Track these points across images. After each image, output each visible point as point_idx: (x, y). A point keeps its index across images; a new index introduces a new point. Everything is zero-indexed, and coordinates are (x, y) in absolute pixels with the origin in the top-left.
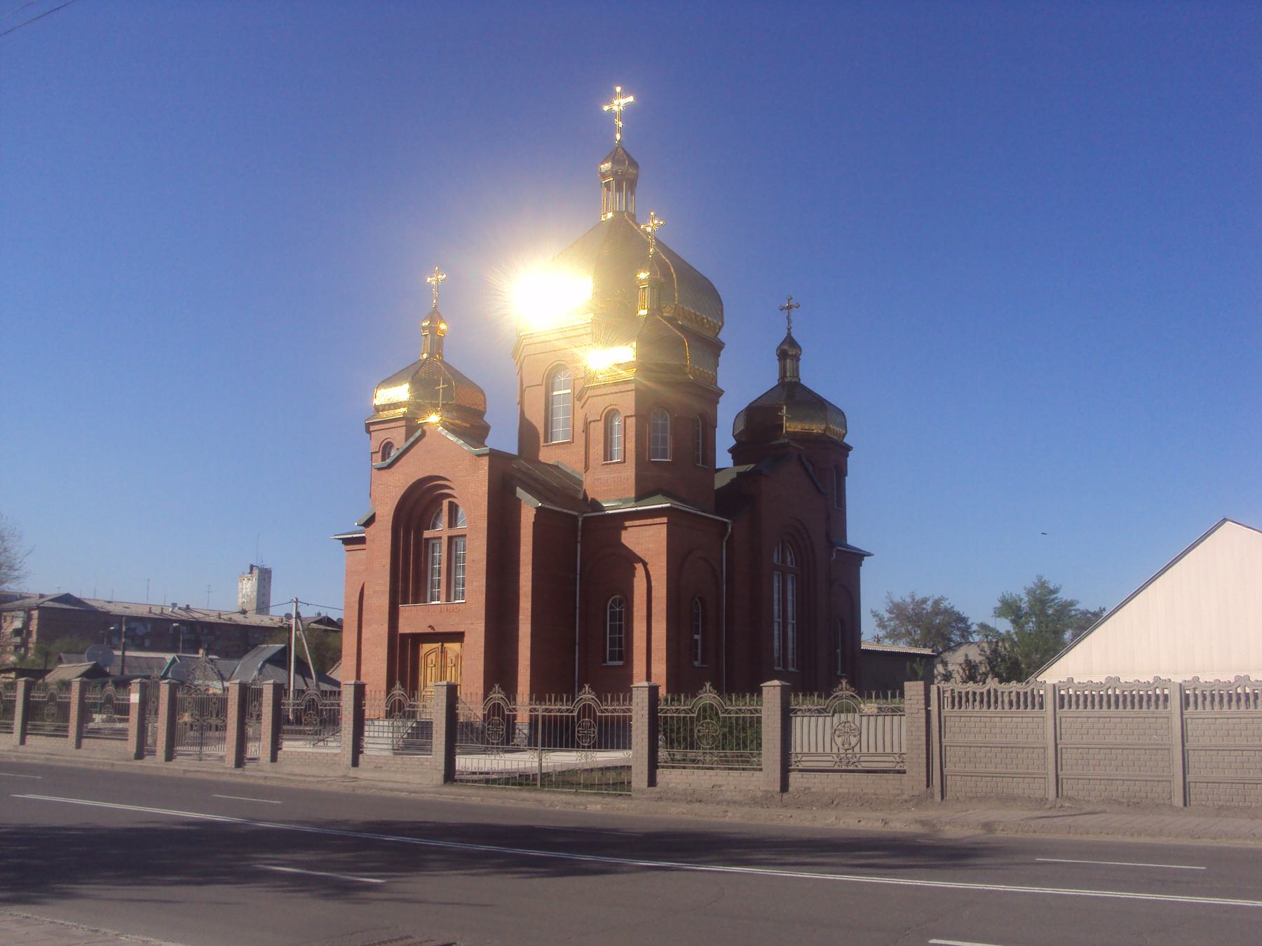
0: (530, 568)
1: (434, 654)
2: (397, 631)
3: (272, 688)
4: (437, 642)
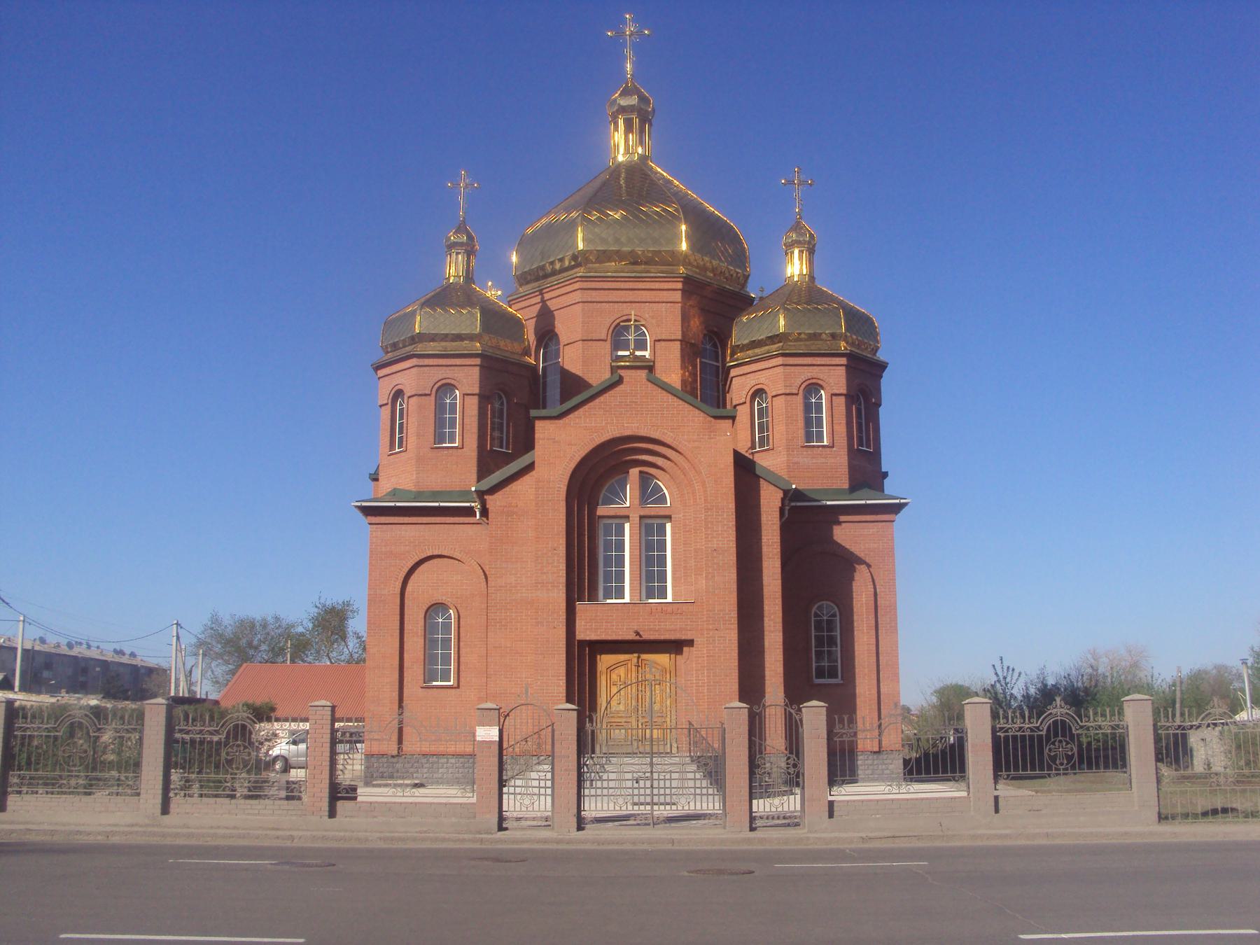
0: (777, 564)
1: (623, 668)
2: (575, 638)
3: (165, 711)
4: (632, 653)
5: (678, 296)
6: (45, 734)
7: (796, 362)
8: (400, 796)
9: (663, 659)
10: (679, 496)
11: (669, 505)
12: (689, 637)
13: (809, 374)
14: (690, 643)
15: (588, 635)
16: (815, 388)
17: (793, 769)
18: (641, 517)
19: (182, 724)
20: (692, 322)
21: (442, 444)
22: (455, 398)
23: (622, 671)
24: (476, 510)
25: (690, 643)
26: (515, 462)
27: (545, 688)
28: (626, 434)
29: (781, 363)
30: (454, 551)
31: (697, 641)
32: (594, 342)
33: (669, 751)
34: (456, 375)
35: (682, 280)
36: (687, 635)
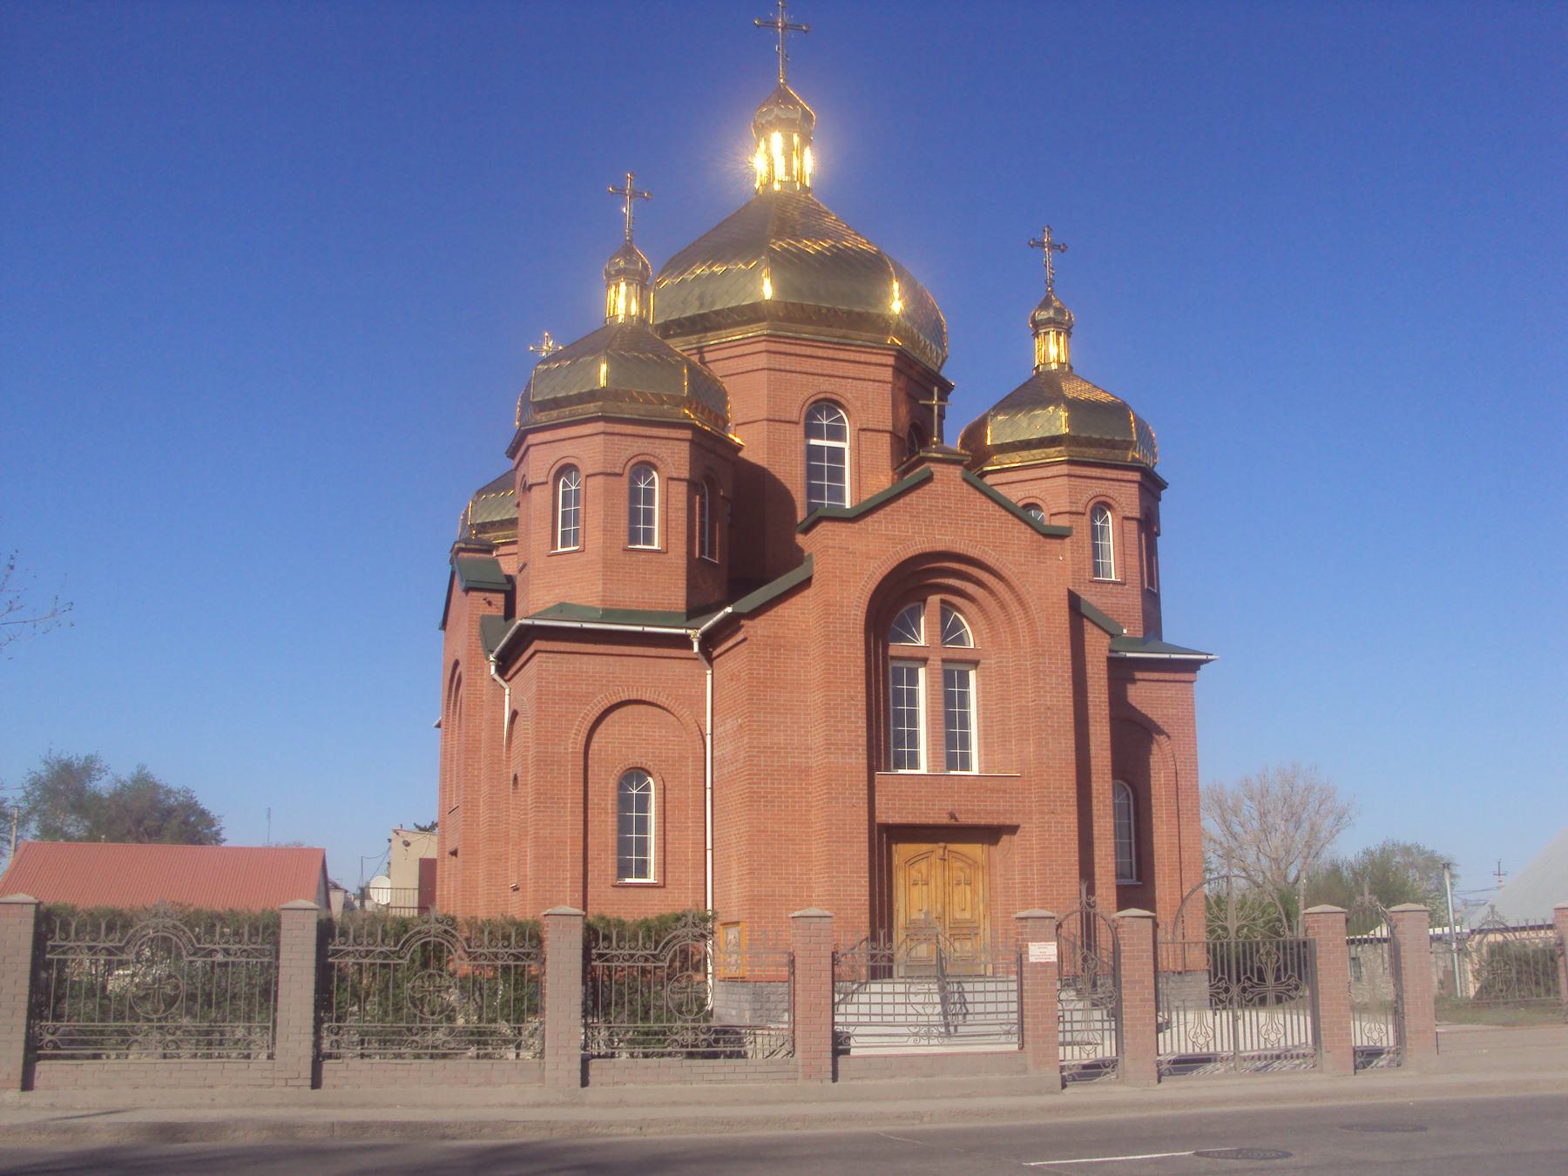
5: (888, 374)
6: (379, 961)
7: (1084, 473)
8: (924, 1046)
9: (975, 850)
10: (989, 635)
11: (972, 647)
12: (1014, 822)
13: (1097, 490)
14: (1012, 829)
15: (892, 817)
16: (1101, 509)
17: (1225, 995)
18: (944, 661)
19: (57, 936)
20: (900, 410)
21: (635, 544)
22: (652, 483)
23: (923, 865)
24: (694, 640)
25: (1012, 829)
26: (784, 577)
27: (842, 889)
28: (938, 549)
29: (1066, 472)
30: (659, 695)
31: (1025, 827)
32: (783, 424)
33: (983, 973)
34: (657, 450)
35: (894, 353)
36: (1012, 819)
